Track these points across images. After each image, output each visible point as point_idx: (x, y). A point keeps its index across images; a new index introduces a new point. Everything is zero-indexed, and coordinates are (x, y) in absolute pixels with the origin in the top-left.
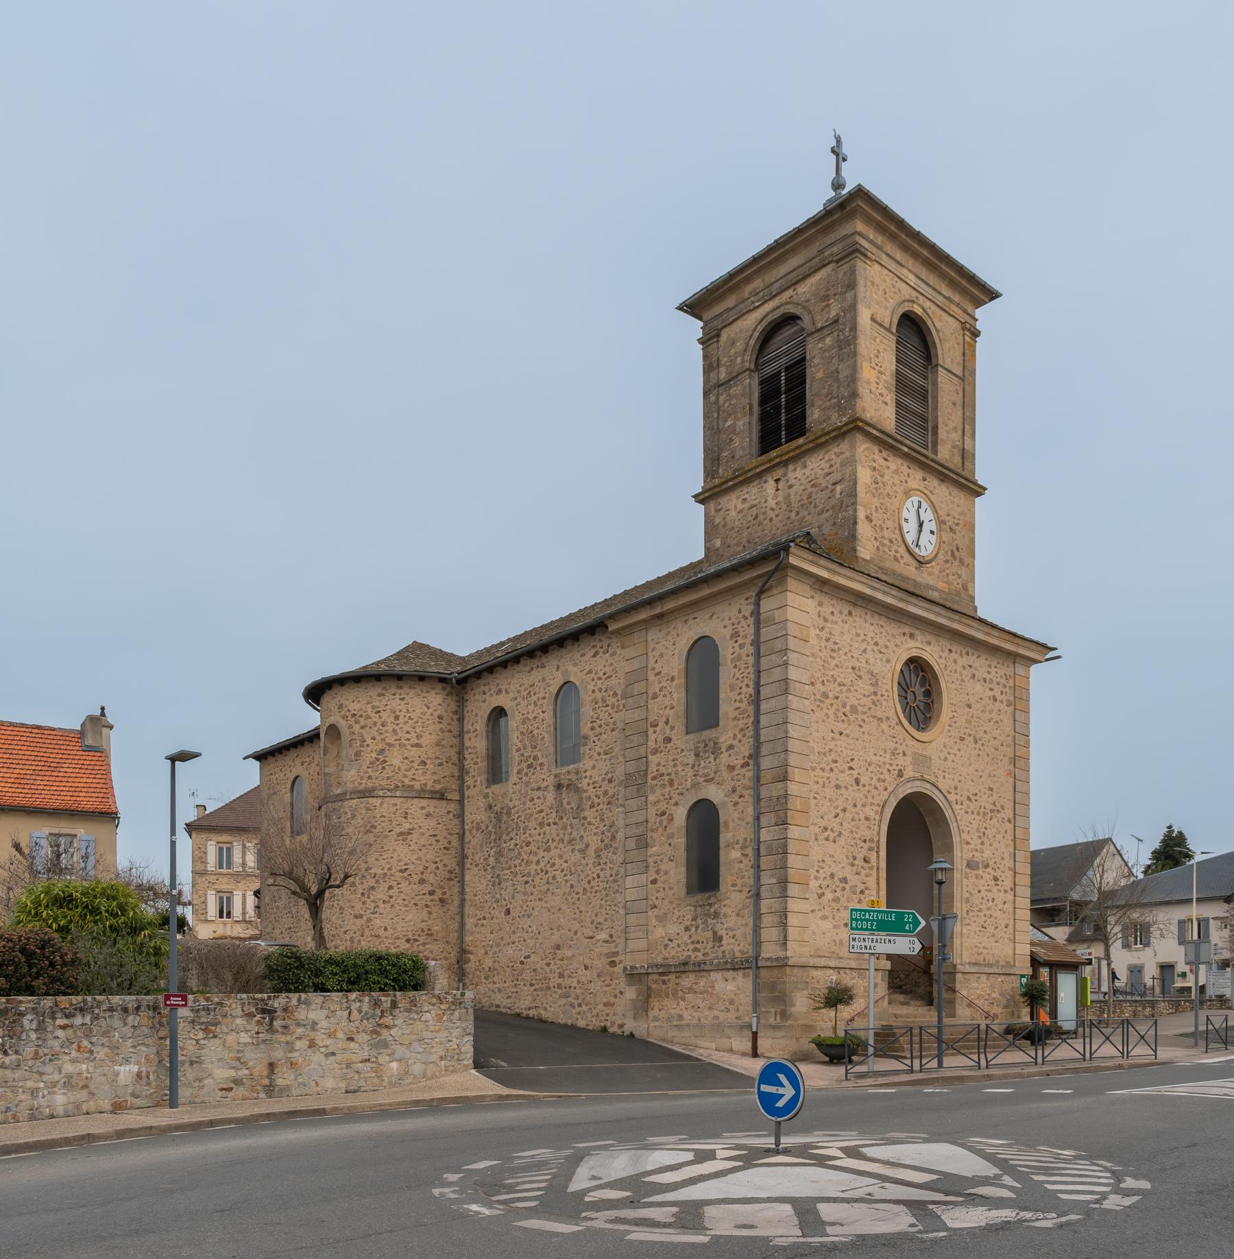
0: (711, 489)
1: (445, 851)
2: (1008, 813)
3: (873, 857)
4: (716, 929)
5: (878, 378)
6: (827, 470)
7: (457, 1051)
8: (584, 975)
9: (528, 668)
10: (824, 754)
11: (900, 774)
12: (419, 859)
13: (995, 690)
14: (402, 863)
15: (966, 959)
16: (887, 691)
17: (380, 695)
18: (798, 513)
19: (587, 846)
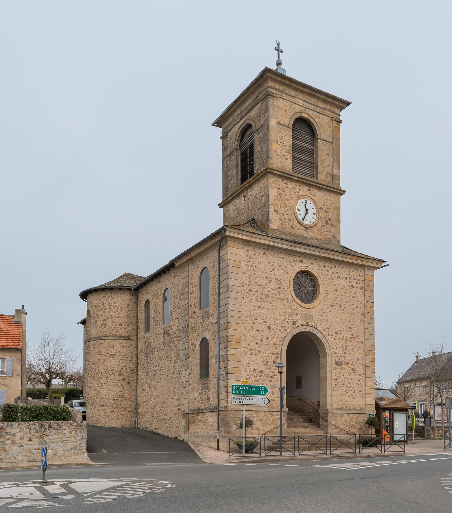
0: (225, 201)
1: (130, 362)
2: (361, 338)
4: (208, 394)
7: (79, 446)
8: (172, 414)
9: (155, 283)
10: (250, 316)
11: (294, 323)
12: (119, 365)
14: (112, 367)
15: (335, 406)
16: (286, 286)
17: (104, 297)
18: (251, 210)
19: (172, 359)
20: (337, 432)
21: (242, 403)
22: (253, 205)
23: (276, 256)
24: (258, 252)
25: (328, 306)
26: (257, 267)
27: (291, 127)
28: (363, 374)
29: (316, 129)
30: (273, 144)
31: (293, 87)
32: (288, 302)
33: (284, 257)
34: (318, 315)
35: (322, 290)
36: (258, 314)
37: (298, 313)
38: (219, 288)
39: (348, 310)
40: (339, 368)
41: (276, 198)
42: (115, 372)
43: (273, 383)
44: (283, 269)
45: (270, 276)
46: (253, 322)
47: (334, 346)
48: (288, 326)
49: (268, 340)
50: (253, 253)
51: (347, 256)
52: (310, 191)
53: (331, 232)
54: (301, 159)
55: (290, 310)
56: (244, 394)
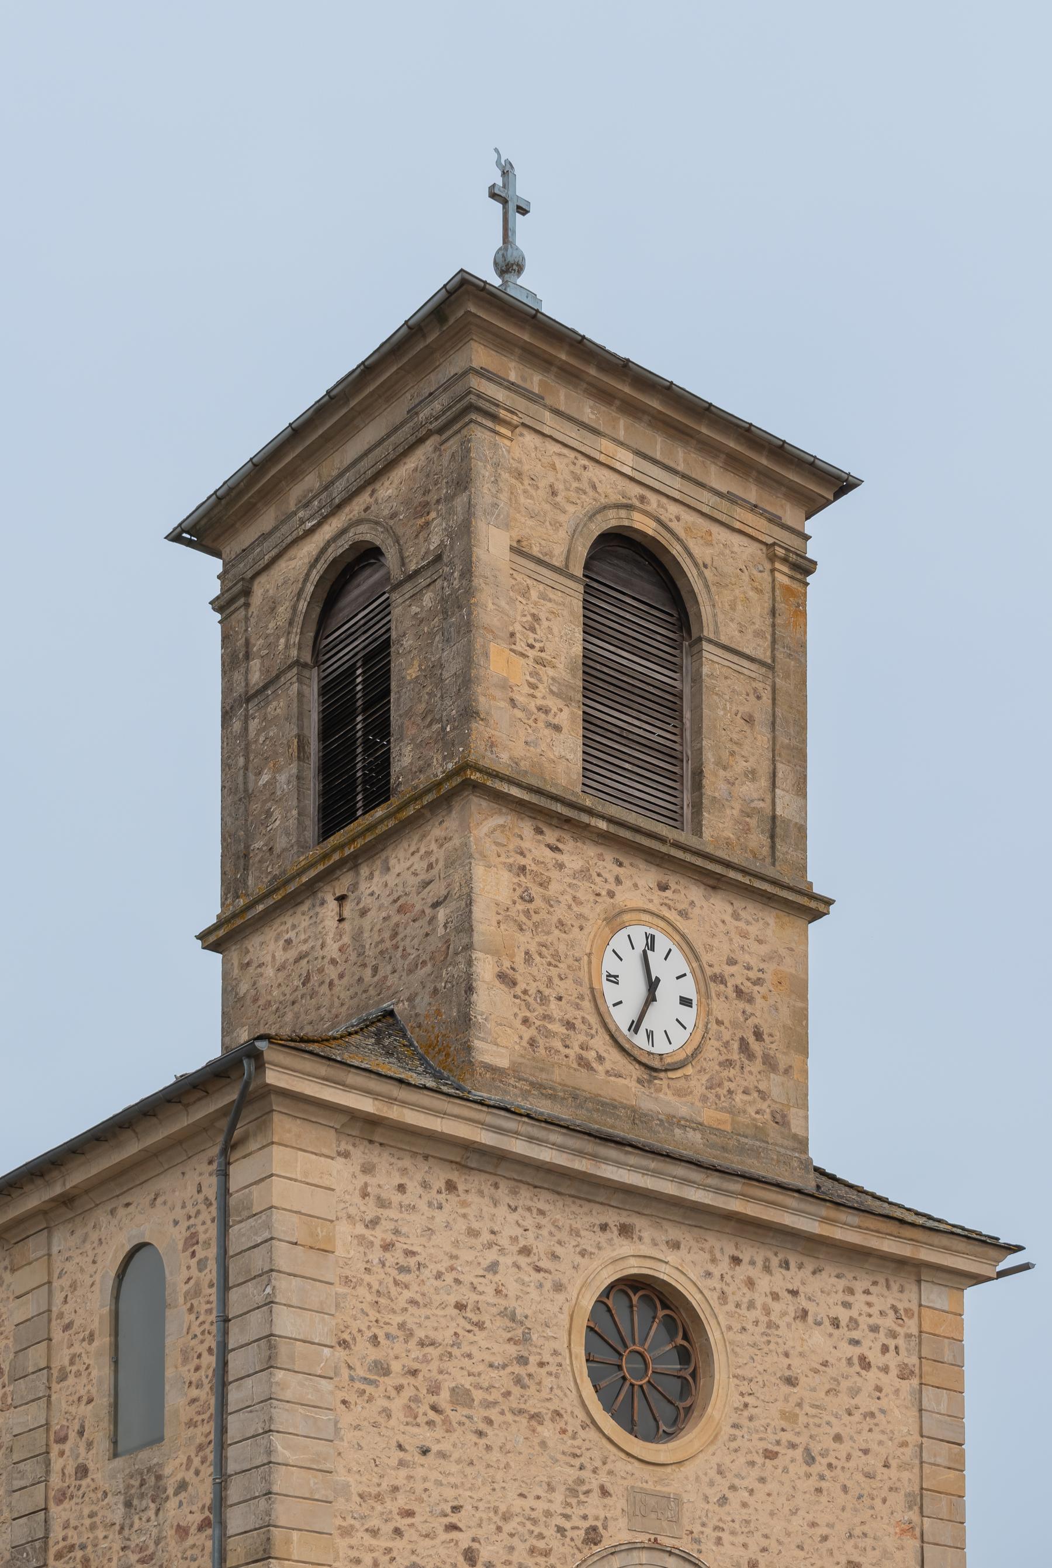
0: (234, 916)
5: (534, 674)
6: (424, 876)
10: (378, 1497)
11: (593, 1536)
13: (866, 1343)
16: (555, 1353)
18: (375, 970)
22: (388, 944)
23: (508, 1200)
24: (419, 1177)
25: (750, 1458)
26: (413, 1254)
27: (579, 572)
29: (692, 591)
30: (493, 647)
31: (589, 384)
32: (564, 1431)
33: (541, 1205)
34: (706, 1499)
35: (724, 1376)
36: (419, 1487)
37: (609, 1488)
38: (223, 1351)
39: (843, 1478)
41: (504, 914)
44: (541, 1264)
46: (390, 1526)
48: (562, 1550)
50: (397, 1180)
51: (843, 1216)
52: (668, 893)
54: (622, 735)
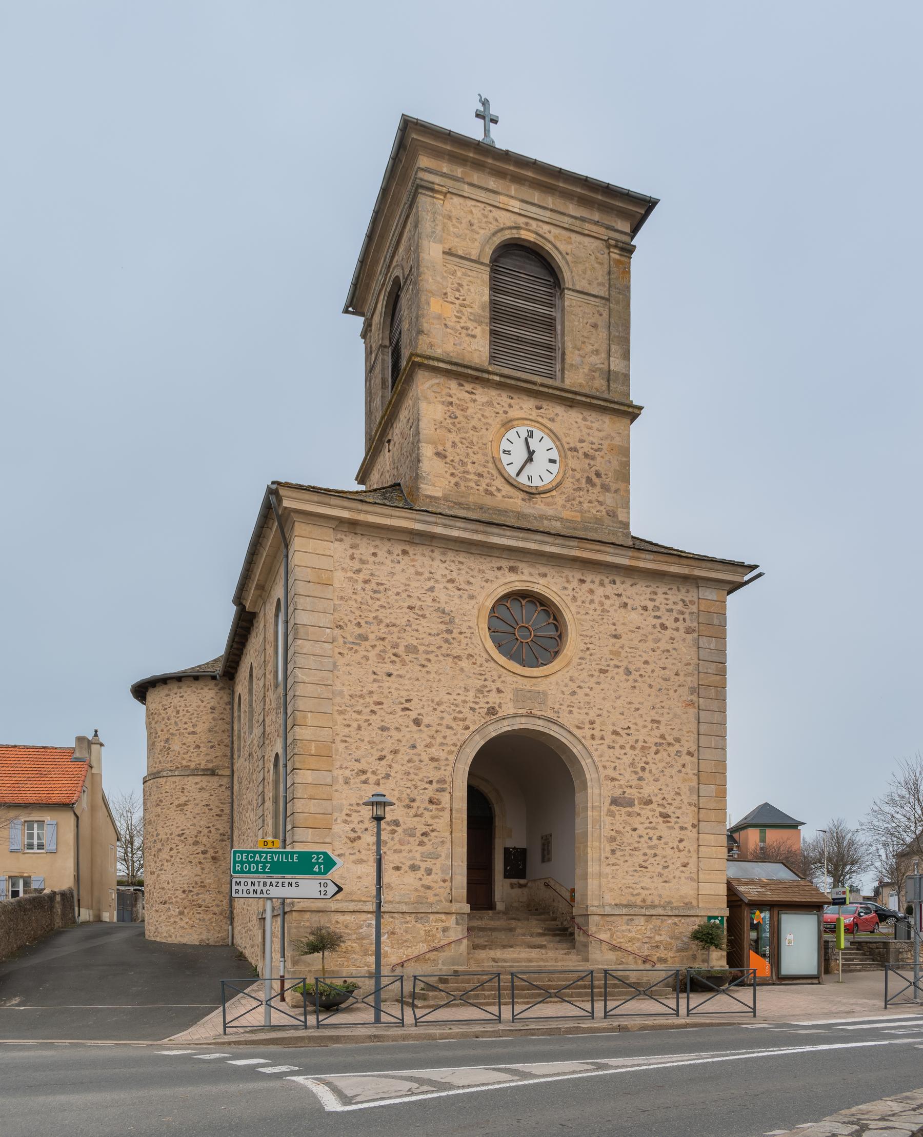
3: (445, 798)
10: (361, 696)
12: (194, 825)
14: (180, 829)
15: (609, 898)
16: (470, 627)
17: (168, 695)
20: (614, 958)
21: (262, 896)
24: (386, 549)
25: (590, 673)
26: (382, 584)
28: (694, 826)
29: (559, 267)
30: (432, 300)
37: (502, 688)
40: (623, 812)
42: (186, 838)
43: (428, 848)
44: (461, 587)
45: (421, 603)
47: (608, 764)
49: (415, 751)
50: (372, 550)
51: (643, 555)
52: (542, 411)
53: (601, 503)
55: (479, 682)
56: (267, 873)
